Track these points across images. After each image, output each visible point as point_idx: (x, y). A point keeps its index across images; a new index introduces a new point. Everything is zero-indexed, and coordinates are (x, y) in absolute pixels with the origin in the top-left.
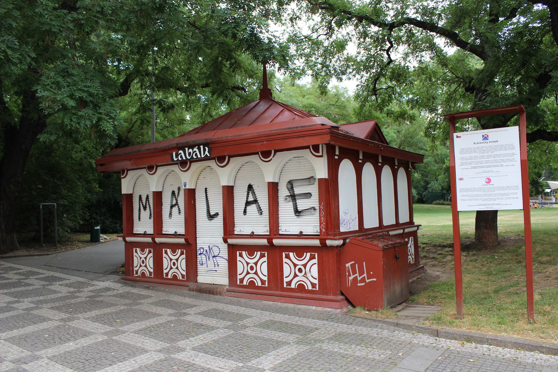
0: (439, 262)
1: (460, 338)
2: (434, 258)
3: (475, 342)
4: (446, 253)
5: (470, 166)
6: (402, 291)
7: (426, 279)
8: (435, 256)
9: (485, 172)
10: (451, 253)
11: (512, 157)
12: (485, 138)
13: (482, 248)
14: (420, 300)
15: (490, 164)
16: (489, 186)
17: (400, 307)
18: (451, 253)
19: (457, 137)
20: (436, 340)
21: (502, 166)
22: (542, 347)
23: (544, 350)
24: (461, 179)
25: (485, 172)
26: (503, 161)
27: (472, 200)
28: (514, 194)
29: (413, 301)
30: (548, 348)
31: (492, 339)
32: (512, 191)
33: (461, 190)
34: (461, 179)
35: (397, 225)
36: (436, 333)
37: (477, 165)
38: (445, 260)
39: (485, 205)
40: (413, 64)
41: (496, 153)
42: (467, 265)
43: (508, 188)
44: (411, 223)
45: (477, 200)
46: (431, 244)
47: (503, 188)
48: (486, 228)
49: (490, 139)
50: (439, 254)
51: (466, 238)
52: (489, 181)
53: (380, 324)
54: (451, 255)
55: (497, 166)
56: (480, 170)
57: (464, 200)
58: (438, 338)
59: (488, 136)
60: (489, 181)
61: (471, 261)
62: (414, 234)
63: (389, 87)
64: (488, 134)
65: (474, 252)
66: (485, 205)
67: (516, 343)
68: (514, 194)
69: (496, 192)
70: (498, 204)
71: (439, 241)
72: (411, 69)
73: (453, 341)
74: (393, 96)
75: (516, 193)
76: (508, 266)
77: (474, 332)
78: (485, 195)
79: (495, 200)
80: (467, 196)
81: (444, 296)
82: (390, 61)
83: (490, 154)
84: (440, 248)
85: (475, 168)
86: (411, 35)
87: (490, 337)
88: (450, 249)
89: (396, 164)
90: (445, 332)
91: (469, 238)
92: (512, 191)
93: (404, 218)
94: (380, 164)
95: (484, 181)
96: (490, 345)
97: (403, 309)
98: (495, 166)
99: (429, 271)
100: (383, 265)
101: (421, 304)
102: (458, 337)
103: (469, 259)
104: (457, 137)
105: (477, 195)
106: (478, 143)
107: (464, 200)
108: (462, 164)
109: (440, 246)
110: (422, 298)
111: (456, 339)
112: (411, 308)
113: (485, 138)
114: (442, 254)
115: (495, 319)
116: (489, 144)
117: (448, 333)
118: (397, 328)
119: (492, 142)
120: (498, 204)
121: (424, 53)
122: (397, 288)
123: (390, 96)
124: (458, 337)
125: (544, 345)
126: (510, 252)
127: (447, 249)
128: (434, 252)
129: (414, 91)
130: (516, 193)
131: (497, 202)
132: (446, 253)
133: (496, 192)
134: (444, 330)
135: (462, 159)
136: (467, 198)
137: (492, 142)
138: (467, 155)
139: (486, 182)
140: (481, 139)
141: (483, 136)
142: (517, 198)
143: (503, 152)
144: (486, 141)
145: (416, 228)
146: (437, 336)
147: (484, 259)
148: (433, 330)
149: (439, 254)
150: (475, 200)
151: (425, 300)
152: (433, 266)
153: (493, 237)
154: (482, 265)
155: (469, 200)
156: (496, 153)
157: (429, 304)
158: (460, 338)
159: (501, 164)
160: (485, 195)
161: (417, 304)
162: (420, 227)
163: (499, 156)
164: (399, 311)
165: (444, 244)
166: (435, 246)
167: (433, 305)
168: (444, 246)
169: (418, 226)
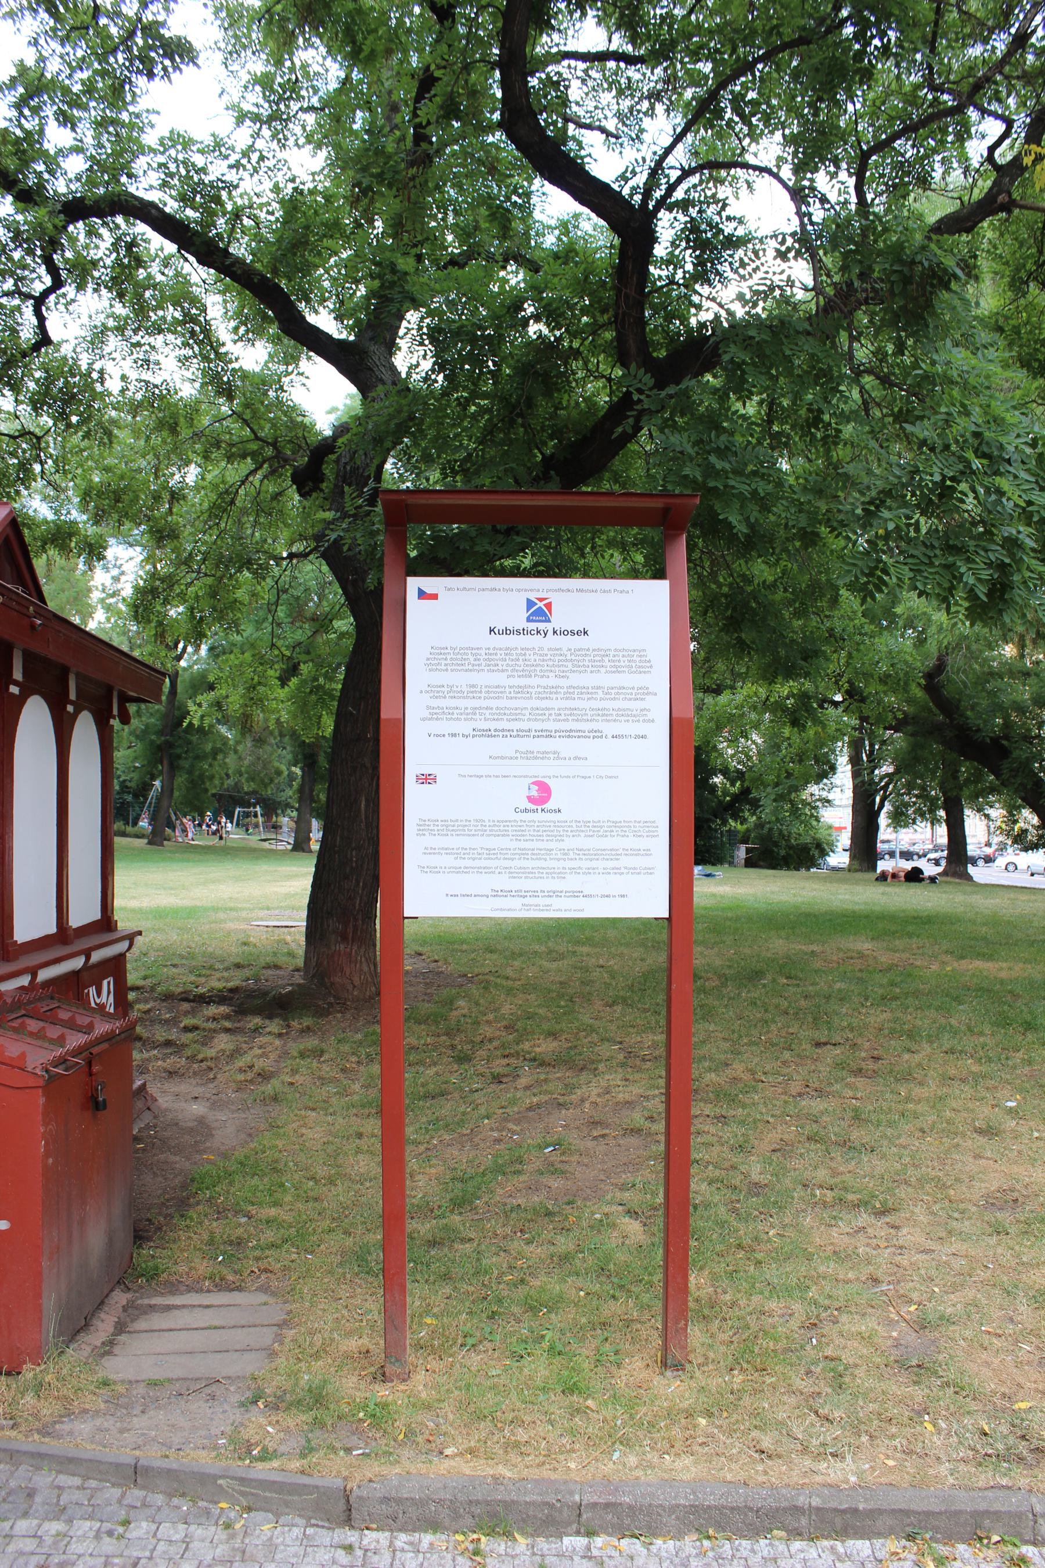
0: (192, 1058)
1: (456, 1516)
2: (168, 1043)
3: (524, 1534)
4: (211, 1025)
5: (466, 727)
6: (110, 1242)
7: (164, 1142)
8: (173, 1035)
9: (528, 755)
10: (228, 1024)
11: (639, 705)
12: (539, 612)
13: (331, 1005)
14: (183, 1268)
15: (551, 726)
16: (540, 816)
17: (104, 1325)
18: (228, 1024)
19: (422, 595)
20: (349, 1548)
21: (598, 735)
22: (796, 1510)
23: (804, 1521)
24: (426, 779)
25: (528, 755)
26: (603, 714)
27: (466, 871)
28: (636, 852)
29: (153, 1275)
30: (818, 1509)
31: (595, 1505)
32: (631, 842)
33: (423, 828)
34: (426, 779)
35: (64, 935)
36: (342, 1505)
37: (500, 725)
38: (211, 1053)
39: (520, 894)
40: (118, 372)
41: (576, 679)
42: (294, 1072)
43: (616, 827)
44: (106, 923)
45: (489, 871)
46: (153, 989)
47: (594, 828)
48: (344, 938)
49: (558, 619)
50: (187, 1029)
51: (268, 967)
52: (542, 793)
53: (43, 1480)
54: (227, 1030)
55: (580, 735)
56: (506, 746)
57: (434, 870)
58: (351, 1536)
59: (549, 606)
60: (542, 793)
61: (302, 1055)
62: (116, 966)
63: (24, 433)
64: (554, 598)
65: (307, 1022)
66: (520, 894)
67: (695, 1509)
68: (636, 852)
69: (568, 843)
70: (575, 894)
71: (181, 980)
72: (114, 385)
73: (427, 1538)
74: (37, 468)
75: (647, 852)
76: (431, 1072)
77: (506, 1473)
78: (523, 853)
79: (561, 875)
80: (448, 851)
81: (270, 1235)
82: (44, 340)
83: (552, 681)
84: (186, 1006)
85: (487, 734)
86: (131, 254)
87: (588, 1498)
88: (223, 1009)
89: (73, 696)
90: (386, 1500)
91: (276, 967)
92: (631, 842)
93: (83, 911)
94: (14, 690)
95: (520, 793)
96: (590, 1534)
97: (121, 1328)
98: (569, 734)
99: (164, 1101)
100: (47, 1154)
101: (190, 1289)
102: (444, 1514)
103: (294, 1047)
104: (422, 595)
105: (490, 853)
106: (506, 631)
107: (434, 870)
108: (435, 714)
109: (185, 997)
110: (184, 1252)
111: (434, 1526)
112: (157, 1321)
113: (539, 612)
114: (196, 1028)
115: (539, 1368)
116: (552, 640)
117: (399, 1501)
118: (136, 1495)
119: (565, 633)
120: (575, 894)
121: (158, 340)
122: (96, 1235)
123: (24, 467)
124: (444, 1514)
125: (802, 1501)
126: (425, 1022)
127: (213, 1010)
128: (167, 1021)
129: (110, 461)
130: (647, 852)
131: (572, 882)
132: (211, 1025)
133: (568, 843)
134: (379, 1490)
135: (435, 691)
136: (449, 861)
137: (565, 633)
138: (461, 679)
139: (530, 799)
140: (519, 618)
141: (530, 604)
142: (649, 871)
143: (605, 679)
144: (542, 626)
145: (123, 946)
146: (348, 1521)
147: (346, 1048)
148: (324, 1494)
149: (187, 1029)
150: (480, 870)
151: (203, 1267)
152: (171, 1074)
153: (365, 968)
154: (344, 1070)
155: (457, 870)
156: (576, 679)
157: (222, 1285)
158: (456, 1516)
159: (594, 726)
160: (523, 853)
161: (173, 1288)
162: (139, 939)
163: (586, 692)
164: (108, 1348)
165: (201, 990)
166: (168, 997)
167: (239, 1289)
168: (203, 1000)
169: (131, 937)
